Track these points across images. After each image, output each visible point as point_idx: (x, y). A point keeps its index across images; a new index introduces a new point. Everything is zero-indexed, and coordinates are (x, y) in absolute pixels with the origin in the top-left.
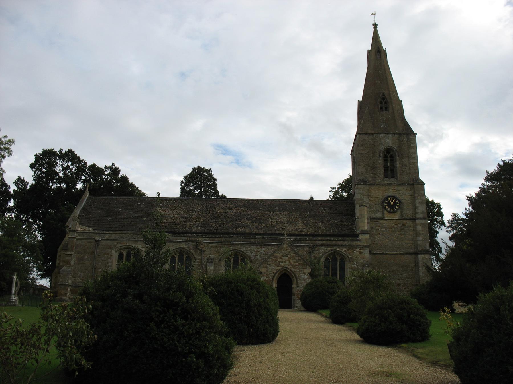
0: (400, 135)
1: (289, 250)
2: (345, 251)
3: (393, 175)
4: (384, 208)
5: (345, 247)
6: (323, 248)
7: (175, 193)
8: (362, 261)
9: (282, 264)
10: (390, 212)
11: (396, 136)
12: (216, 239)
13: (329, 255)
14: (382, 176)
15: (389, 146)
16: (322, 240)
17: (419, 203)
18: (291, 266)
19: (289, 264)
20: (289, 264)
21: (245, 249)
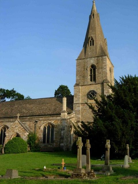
0: (98, 57)
1: (18, 124)
2: (53, 122)
3: (95, 80)
4: (88, 98)
5: (53, 120)
6: (42, 121)
7: (54, 96)
8: (61, 127)
9: (15, 131)
10: (90, 99)
11: (96, 58)
12: (5, 120)
13: (47, 124)
14: (89, 80)
15: (92, 64)
16: (42, 117)
17: (106, 93)
18: (19, 132)
19: (18, 131)
20: (18, 131)
21: (8, 124)
